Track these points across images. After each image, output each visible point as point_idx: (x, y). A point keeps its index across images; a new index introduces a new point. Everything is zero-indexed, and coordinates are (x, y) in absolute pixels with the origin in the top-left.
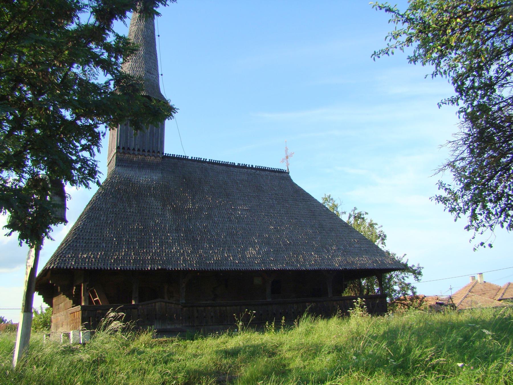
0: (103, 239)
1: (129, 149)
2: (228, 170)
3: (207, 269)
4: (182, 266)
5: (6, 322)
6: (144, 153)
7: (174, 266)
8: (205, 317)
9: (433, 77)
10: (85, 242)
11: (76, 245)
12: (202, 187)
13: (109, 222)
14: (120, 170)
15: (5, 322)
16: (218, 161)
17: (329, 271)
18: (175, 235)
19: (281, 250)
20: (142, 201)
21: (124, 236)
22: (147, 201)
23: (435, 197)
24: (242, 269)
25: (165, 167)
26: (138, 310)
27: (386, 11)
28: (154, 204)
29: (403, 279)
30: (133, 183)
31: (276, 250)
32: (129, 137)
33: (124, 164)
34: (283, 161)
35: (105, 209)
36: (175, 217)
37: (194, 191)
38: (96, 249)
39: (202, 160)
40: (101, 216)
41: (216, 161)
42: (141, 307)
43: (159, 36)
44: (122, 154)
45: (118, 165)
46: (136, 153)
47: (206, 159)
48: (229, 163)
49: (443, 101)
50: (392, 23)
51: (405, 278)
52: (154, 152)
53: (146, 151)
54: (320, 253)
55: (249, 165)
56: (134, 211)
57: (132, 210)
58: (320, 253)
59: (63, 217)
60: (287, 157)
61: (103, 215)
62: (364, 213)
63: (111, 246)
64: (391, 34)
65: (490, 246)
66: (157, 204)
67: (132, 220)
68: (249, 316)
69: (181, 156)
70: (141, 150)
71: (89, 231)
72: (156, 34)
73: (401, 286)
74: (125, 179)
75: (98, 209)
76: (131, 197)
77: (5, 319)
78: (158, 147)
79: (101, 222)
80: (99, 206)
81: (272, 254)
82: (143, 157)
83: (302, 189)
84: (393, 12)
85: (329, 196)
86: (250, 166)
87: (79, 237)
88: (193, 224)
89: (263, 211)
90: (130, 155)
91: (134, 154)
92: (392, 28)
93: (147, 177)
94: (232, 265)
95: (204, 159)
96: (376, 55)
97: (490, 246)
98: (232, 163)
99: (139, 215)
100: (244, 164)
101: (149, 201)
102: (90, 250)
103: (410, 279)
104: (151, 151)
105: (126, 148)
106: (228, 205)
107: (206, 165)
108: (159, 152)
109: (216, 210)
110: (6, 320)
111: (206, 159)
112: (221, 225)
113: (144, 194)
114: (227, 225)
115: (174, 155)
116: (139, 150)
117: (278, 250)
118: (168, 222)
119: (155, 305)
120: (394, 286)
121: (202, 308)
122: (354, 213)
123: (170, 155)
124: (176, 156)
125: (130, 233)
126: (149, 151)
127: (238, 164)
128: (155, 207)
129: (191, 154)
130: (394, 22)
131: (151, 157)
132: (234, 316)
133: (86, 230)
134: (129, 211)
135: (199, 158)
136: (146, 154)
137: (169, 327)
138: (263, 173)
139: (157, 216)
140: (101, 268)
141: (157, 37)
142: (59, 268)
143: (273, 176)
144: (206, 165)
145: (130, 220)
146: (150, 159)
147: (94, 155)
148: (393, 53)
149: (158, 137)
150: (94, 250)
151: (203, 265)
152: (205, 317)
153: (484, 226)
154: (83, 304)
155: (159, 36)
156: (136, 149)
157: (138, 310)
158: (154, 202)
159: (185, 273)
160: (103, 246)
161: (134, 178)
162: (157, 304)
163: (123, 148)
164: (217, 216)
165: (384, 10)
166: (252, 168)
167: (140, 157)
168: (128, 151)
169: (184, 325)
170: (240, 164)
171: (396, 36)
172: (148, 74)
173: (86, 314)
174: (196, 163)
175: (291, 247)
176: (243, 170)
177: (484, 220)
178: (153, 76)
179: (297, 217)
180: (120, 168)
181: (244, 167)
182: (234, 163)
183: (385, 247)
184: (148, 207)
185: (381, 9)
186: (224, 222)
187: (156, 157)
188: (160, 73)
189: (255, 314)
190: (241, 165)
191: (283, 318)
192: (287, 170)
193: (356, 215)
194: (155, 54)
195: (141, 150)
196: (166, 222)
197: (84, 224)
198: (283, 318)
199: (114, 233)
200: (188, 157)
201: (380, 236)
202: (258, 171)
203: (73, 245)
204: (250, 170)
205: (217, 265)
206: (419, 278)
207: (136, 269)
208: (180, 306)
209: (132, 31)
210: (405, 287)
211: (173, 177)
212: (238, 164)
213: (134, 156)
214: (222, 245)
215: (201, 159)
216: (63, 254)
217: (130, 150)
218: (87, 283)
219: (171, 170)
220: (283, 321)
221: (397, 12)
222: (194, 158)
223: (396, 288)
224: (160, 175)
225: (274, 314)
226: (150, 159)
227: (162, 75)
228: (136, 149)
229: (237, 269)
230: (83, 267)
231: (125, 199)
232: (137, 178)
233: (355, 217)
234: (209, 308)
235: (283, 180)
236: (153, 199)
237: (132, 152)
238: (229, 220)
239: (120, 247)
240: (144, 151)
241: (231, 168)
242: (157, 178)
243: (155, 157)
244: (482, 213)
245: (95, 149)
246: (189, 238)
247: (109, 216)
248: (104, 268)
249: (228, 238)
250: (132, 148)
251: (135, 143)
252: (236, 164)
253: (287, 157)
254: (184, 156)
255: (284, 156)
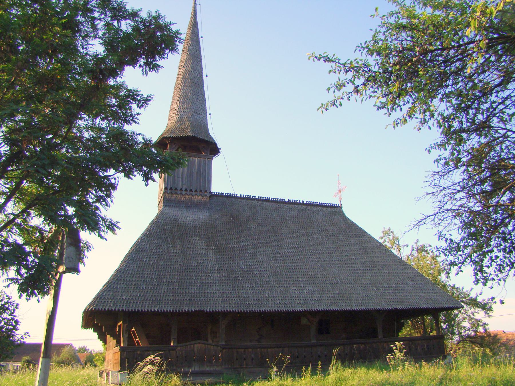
0: (144, 280)
1: (176, 189)
2: (278, 206)
3: (247, 311)
4: (220, 308)
5: (89, 351)
6: (191, 192)
7: (212, 307)
8: (245, 359)
9: (394, 127)
10: (126, 284)
11: (117, 287)
12: (250, 225)
13: (151, 263)
14: (168, 210)
15: (88, 351)
16: (267, 198)
17: (378, 311)
18: (216, 275)
19: (326, 289)
20: (186, 241)
21: (164, 278)
22: (191, 241)
23: (436, 248)
24: (283, 310)
25: (213, 206)
26: (176, 352)
27: (325, 61)
28: (198, 245)
29: (473, 315)
30: (180, 223)
31: (322, 289)
32: (176, 178)
33: (172, 205)
34: (336, 196)
35: (149, 250)
36: (218, 257)
37: (241, 229)
38: (136, 290)
39: (251, 197)
40: (144, 257)
41: (265, 198)
42: (179, 348)
43: (207, 76)
44: (170, 195)
45: (166, 206)
46: (184, 193)
47: (255, 197)
48: (279, 200)
49: (432, 145)
50: (332, 74)
51: (475, 314)
52: (201, 191)
53: (194, 190)
54: (369, 292)
55: (300, 201)
56: (177, 252)
57: (175, 251)
58: (369, 292)
59: (77, 267)
60: (340, 191)
61: (146, 256)
62: (428, 245)
63: (151, 288)
64: (335, 84)
65: (502, 302)
66: (201, 244)
67: (175, 260)
68: (283, 362)
69: (230, 194)
70: (188, 191)
71: (131, 272)
72: (204, 74)
73: (471, 322)
74: (172, 220)
75: (142, 250)
76: (176, 237)
77: (87, 348)
78: (205, 186)
79: (144, 263)
80: (143, 247)
81: (317, 294)
82: (191, 196)
83: (355, 224)
84: (333, 62)
85: (389, 229)
86: (301, 202)
87: (120, 278)
88: (237, 263)
89: (311, 248)
90: (177, 196)
91: (181, 194)
92: (334, 78)
93: (194, 216)
94: (273, 306)
95: (253, 196)
96: (324, 107)
97: (502, 302)
98: (282, 199)
99: (182, 255)
100: (295, 200)
101: (193, 241)
102: (129, 291)
103: (480, 314)
104: (198, 190)
105: (173, 189)
106: (274, 243)
107: (255, 202)
108: (206, 191)
109: (262, 249)
110: (89, 349)
111: (255, 197)
112: (265, 264)
113: (199, 232)
114: (272, 264)
115: (223, 193)
116: (186, 190)
117: (324, 289)
118: (211, 262)
119: (194, 347)
120: (463, 322)
121: (242, 350)
122: (416, 245)
123: (219, 193)
124: (224, 194)
125: (172, 274)
126: (196, 191)
127: (288, 200)
128: (199, 247)
129: (240, 192)
130: (335, 72)
131: (198, 196)
132: (268, 361)
133: (128, 272)
134: (172, 251)
135: (248, 196)
136: (194, 193)
137: (208, 369)
138: (314, 209)
139: (200, 256)
140: (138, 310)
141: (205, 78)
142: (97, 309)
143: (324, 211)
144: (255, 202)
145: (172, 260)
146: (198, 198)
147: (110, 205)
148: (341, 105)
149: (205, 176)
150: (133, 292)
151: (242, 306)
152: (245, 359)
153: (493, 279)
154: (122, 345)
155: (207, 76)
156: (184, 190)
157: (176, 352)
158: (199, 242)
159: (225, 314)
160: (143, 288)
161: (181, 218)
162: (196, 346)
163: (171, 189)
164: (262, 255)
165: (322, 59)
166: (303, 204)
167: (187, 197)
168: (176, 191)
169: (223, 367)
170: (290, 200)
171: (340, 86)
172: (195, 115)
173: (125, 355)
174: (245, 200)
175: (338, 286)
176: (294, 206)
177: (493, 273)
178: (200, 116)
179: (347, 254)
180: (167, 208)
181: (295, 203)
182: (284, 199)
183: (449, 281)
184: (192, 247)
185: (319, 60)
186: (269, 261)
187: (203, 197)
188: (208, 113)
189: (289, 359)
190: (291, 201)
191: (320, 363)
192: (339, 204)
193: (419, 248)
194: (202, 95)
195: (188, 191)
196: (209, 262)
197: (126, 266)
198: (320, 363)
199: (155, 274)
200: (237, 195)
201: (445, 269)
202: (309, 207)
203: (114, 287)
204: (301, 206)
205: (256, 306)
206: (490, 314)
207: (173, 311)
208: (219, 348)
209: (180, 73)
210: (476, 323)
211: (220, 215)
212: (288, 200)
213: (182, 196)
214: (264, 285)
215: (250, 196)
216: (103, 295)
217: (177, 190)
218: (126, 325)
219: (219, 209)
220: (319, 366)
221: (337, 61)
222: (243, 195)
223: (466, 324)
224: (207, 214)
225: (319, 356)
226: (198, 198)
227: (210, 114)
228: (184, 190)
229: (278, 310)
230: (121, 309)
231: (169, 240)
232: (183, 218)
233: (418, 250)
234: (250, 350)
235: (335, 214)
236: (198, 239)
237: (179, 192)
238: (274, 258)
239: (160, 288)
240: (191, 190)
241: (282, 205)
242: (204, 217)
243: (202, 196)
244: (489, 265)
245: (109, 200)
246: (231, 279)
247: (152, 257)
248: (142, 310)
249: (271, 277)
250: (179, 189)
251: (182, 182)
252: (287, 201)
253: (340, 191)
254: (232, 194)
255: (337, 191)
